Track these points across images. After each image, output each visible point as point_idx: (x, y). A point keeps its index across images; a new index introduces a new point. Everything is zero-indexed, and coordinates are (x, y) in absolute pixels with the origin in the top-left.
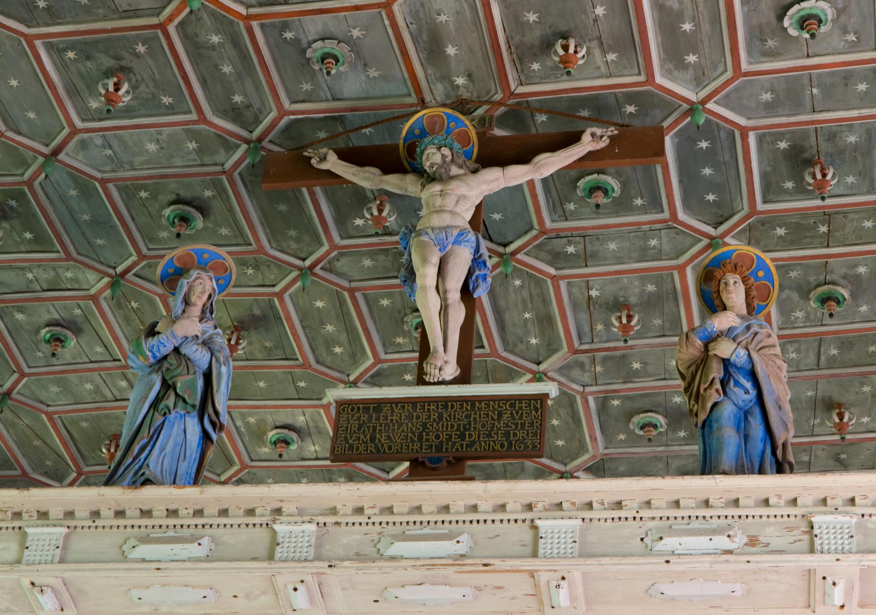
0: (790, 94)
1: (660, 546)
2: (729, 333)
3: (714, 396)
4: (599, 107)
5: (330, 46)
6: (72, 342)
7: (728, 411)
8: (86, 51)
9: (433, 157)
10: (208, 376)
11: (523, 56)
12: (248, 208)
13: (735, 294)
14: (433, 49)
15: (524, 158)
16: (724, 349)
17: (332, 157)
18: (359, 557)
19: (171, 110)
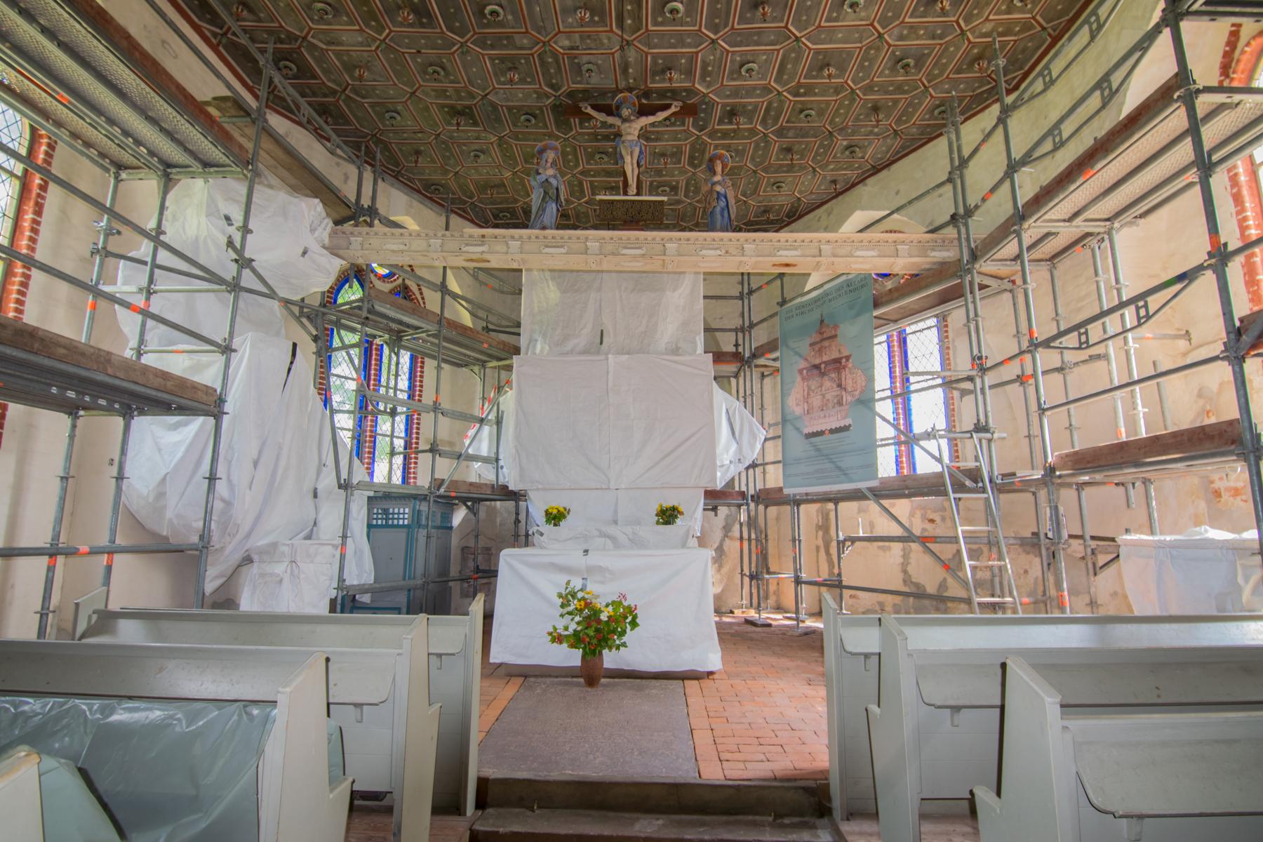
0: (736, 92)
2: (718, 182)
3: (715, 204)
4: (674, 93)
5: (590, 66)
6: (482, 156)
7: (718, 209)
8: (503, 59)
9: (625, 112)
11: (654, 74)
12: (550, 118)
13: (719, 168)
14: (625, 70)
15: (653, 114)
16: (718, 188)
18: (613, 254)
19: (530, 83)
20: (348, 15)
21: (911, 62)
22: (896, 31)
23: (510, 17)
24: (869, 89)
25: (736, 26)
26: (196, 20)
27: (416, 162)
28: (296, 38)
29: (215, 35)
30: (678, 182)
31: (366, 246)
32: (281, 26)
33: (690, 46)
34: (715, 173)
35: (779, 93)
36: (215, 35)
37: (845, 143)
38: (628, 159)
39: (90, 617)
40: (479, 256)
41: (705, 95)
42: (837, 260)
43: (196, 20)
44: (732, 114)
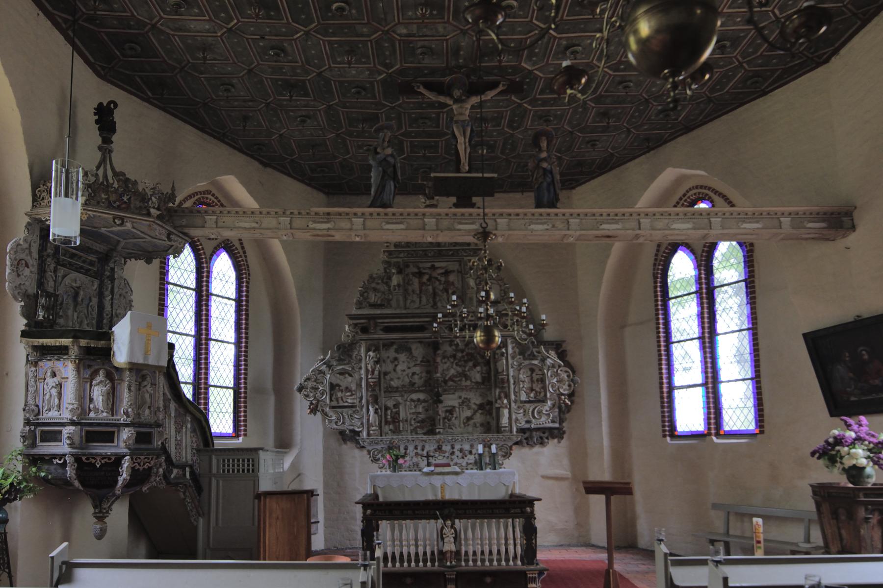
1: (530, 227)
2: (545, 159)
9: (457, 93)
10: (394, 166)
13: (544, 144)
16: (545, 165)
17: (421, 87)
18: (449, 229)
19: (364, 63)
20: (199, 8)
21: (728, 44)
23: (354, 11)
25: (565, 18)
26: (50, 9)
27: (244, 127)
30: (495, 141)
31: (220, 224)
32: (133, 15)
33: (520, 33)
34: (540, 150)
36: (66, 21)
37: (660, 108)
38: (461, 140)
39: (61, 567)
40: (325, 232)
41: (530, 72)
43: (50, 9)
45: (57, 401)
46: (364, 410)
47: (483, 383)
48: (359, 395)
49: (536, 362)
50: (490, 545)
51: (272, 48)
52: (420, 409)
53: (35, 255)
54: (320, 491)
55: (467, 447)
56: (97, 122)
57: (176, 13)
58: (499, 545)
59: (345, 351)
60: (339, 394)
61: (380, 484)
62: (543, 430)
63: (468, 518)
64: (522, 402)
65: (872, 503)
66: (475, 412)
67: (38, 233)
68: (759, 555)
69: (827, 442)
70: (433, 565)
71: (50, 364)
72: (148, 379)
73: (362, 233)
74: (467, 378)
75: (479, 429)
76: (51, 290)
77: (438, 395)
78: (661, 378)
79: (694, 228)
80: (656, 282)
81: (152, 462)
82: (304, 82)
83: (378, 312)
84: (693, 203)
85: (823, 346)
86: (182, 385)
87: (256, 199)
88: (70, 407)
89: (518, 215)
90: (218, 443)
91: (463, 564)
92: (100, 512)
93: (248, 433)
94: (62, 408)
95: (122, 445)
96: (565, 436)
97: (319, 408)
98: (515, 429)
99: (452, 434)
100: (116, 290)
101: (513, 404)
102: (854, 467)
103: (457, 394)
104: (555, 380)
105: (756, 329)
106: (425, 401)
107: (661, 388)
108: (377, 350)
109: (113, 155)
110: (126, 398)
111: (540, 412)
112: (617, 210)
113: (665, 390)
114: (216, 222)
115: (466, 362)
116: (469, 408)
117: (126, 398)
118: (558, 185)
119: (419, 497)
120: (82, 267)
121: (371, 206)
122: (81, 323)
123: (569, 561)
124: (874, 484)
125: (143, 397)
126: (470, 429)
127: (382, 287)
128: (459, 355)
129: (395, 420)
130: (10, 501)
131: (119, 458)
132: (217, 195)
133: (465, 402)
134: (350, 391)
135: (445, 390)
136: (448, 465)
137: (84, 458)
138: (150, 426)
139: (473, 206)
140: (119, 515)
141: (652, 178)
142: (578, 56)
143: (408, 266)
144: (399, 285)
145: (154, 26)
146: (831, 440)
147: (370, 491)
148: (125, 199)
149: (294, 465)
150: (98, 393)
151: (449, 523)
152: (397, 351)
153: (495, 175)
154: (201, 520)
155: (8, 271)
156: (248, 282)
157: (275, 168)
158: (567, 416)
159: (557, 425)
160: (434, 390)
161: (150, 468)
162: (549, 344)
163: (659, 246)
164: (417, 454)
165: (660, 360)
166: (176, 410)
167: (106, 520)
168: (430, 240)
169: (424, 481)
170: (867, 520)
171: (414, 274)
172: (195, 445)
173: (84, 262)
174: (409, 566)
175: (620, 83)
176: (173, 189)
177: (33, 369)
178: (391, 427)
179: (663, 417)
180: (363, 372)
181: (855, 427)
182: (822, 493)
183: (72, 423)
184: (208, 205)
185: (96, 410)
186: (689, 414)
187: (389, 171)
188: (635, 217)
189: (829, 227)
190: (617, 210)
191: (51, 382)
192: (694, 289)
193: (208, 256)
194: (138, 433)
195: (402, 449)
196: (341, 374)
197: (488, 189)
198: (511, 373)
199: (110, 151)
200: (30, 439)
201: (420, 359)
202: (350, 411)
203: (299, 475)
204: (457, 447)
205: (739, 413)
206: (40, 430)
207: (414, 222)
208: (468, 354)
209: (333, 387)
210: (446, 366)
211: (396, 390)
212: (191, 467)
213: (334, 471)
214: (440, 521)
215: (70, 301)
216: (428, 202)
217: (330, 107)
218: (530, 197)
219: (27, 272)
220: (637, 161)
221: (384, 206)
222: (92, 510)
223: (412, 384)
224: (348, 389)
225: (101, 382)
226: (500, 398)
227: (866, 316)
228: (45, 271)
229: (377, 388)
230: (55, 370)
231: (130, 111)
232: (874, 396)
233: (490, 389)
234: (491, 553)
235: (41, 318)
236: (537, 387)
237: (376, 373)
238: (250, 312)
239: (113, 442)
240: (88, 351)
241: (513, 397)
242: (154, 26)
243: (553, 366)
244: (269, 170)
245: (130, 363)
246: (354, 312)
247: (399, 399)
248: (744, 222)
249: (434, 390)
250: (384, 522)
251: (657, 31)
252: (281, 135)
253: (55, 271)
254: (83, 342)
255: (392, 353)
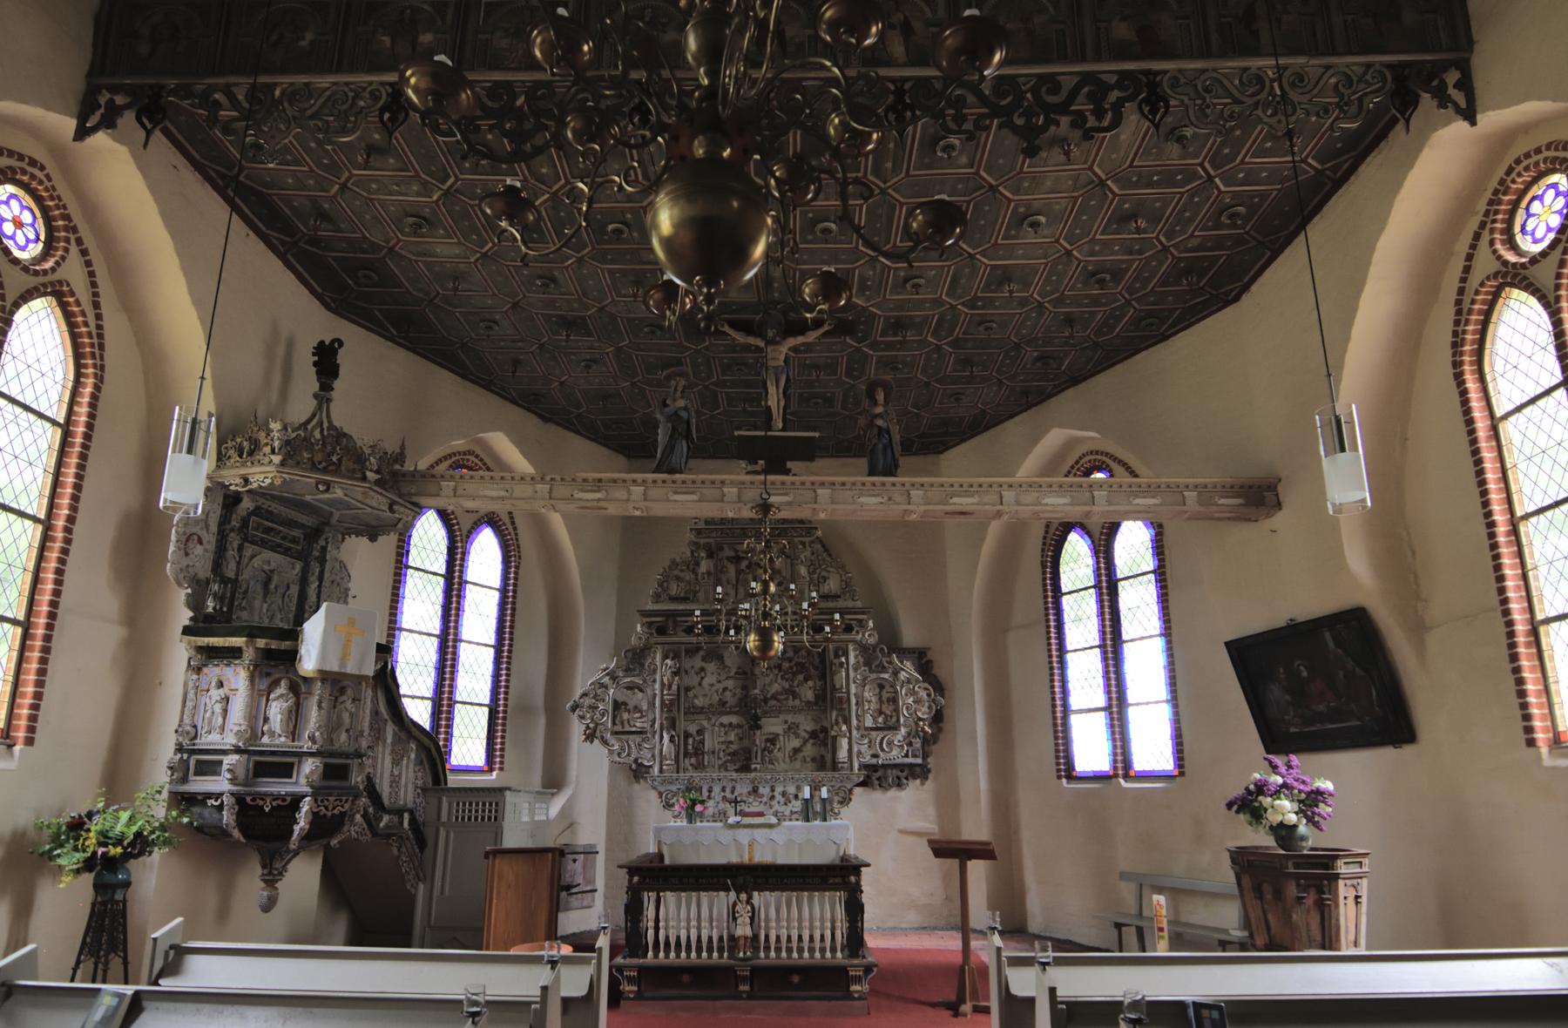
2: (879, 416)
10: (688, 422)
13: (880, 397)
16: (880, 422)
20: (445, 228)
21: (1108, 277)
22: (1086, 248)
24: (1059, 302)
28: (380, 248)
29: (283, 243)
32: (364, 237)
35: (953, 307)
36: (283, 243)
38: (772, 389)
39: (167, 953)
41: (865, 309)
42: (1020, 508)
44: (898, 325)
45: (220, 720)
46: (657, 737)
47: (816, 703)
48: (651, 717)
49: (886, 676)
50: (800, 928)
51: (540, 277)
52: (732, 737)
53: (214, 528)
54: (601, 848)
55: (791, 790)
56: (315, 364)
57: (415, 234)
58: (822, 928)
59: (636, 659)
60: (625, 716)
61: (666, 839)
62: (901, 767)
63: (782, 890)
64: (867, 729)
65: (1305, 876)
66: (805, 742)
67: (220, 500)
68: (1162, 951)
69: (1247, 789)
70: (721, 957)
71: (217, 670)
72: (349, 692)
73: (642, 504)
74: (795, 696)
75: (810, 765)
76: (231, 574)
77: (756, 718)
78: (1053, 699)
79: (1071, 504)
80: (1044, 573)
81: (347, 806)
82: (583, 318)
83: (681, 607)
84: (1088, 473)
85: (1251, 657)
86: (404, 700)
87: (531, 462)
88: (236, 729)
89: (843, 484)
90: (454, 780)
91: (762, 955)
92: (270, 873)
93: (505, 766)
94: (224, 732)
95: (303, 781)
96: (931, 776)
97: (598, 734)
98: (856, 766)
99: (774, 771)
100: (327, 575)
101: (854, 732)
102: (1281, 824)
103: (782, 717)
104: (910, 700)
105: (390, 629)
106: (739, 726)
107: (1054, 712)
108: (676, 656)
109: (332, 405)
110: (313, 718)
111: (890, 743)
112: (971, 480)
113: (1059, 715)
114: (455, 490)
115: (794, 674)
116: (797, 736)
117: (313, 718)
118: (898, 449)
119: (719, 859)
120: (279, 545)
121: (656, 471)
122: (271, 618)
123: (928, 951)
124: (1312, 849)
125: (339, 717)
126: (798, 764)
127: (689, 576)
128: (786, 665)
129: (698, 751)
130: (136, 857)
131: (296, 800)
132: (482, 455)
133: (792, 729)
134: (640, 711)
135: (765, 712)
136: (761, 814)
137: (248, 799)
138: (347, 756)
139: (787, 472)
140: (303, 877)
141: (1036, 441)
142: (921, 290)
143: (721, 549)
144: (709, 573)
145: (391, 250)
146: (1252, 787)
147: (652, 849)
148: (334, 459)
149: (565, 812)
150: (276, 710)
151: (744, 896)
152: (704, 659)
153: (817, 434)
154: (421, 886)
155: (172, 548)
156: (517, 567)
157: (557, 424)
158: (933, 748)
159: (919, 761)
160: (751, 712)
161: (343, 814)
162: (904, 653)
163: (1047, 526)
164: (724, 798)
165: (1052, 674)
166: (395, 734)
167: (278, 885)
168: (731, 515)
169: (727, 836)
170: (1300, 899)
171: (728, 559)
172: (420, 783)
173: (284, 538)
174: (688, 956)
175: (980, 324)
176: (403, 447)
177: (195, 677)
178: (693, 760)
179: (1057, 751)
180: (657, 686)
181: (1283, 769)
182: (1243, 859)
183: (237, 750)
184: (470, 469)
185: (272, 734)
186: (1091, 749)
187: (680, 427)
188: (995, 488)
189: (1247, 504)
190: (971, 480)
191: (216, 694)
192: (1092, 583)
193: (464, 533)
194: (326, 766)
195: (705, 791)
196: (629, 688)
197: (807, 451)
198: (853, 689)
199: (329, 400)
200: (181, 771)
201: (734, 670)
202: (638, 738)
203: (572, 825)
204: (779, 789)
205: (1153, 749)
206: (195, 759)
207: (710, 492)
208: (797, 664)
209: (617, 705)
210: (767, 680)
211: (701, 711)
212: (411, 812)
213: (621, 817)
214: (733, 894)
215: (259, 588)
216: (750, 468)
217: (619, 349)
218: (863, 463)
219: (199, 550)
220: (1016, 419)
221: (672, 471)
222: (259, 870)
223: (723, 703)
224: (637, 709)
225: (282, 696)
226: (837, 723)
227: (1301, 619)
228: (225, 550)
229: (675, 709)
230: (223, 679)
231: (364, 353)
232: (1318, 727)
233: (825, 711)
234: (800, 938)
235: (210, 610)
236: (888, 709)
237: (674, 687)
238: (518, 606)
239: (290, 777)
240: (268, 655)
241: (854, 722)
242: (391, 250)
243: (909, 682)
244: (552, 427)
245: (320, 671)
246: (651, 607)
247: (705, 723)
248: (1137, 496)
249: (751, 712)
250: (668, 893)
251: (678, 226)
252: (562, 384)
253: (240, 548)
254: (261, 643)
255: (697, 662)
